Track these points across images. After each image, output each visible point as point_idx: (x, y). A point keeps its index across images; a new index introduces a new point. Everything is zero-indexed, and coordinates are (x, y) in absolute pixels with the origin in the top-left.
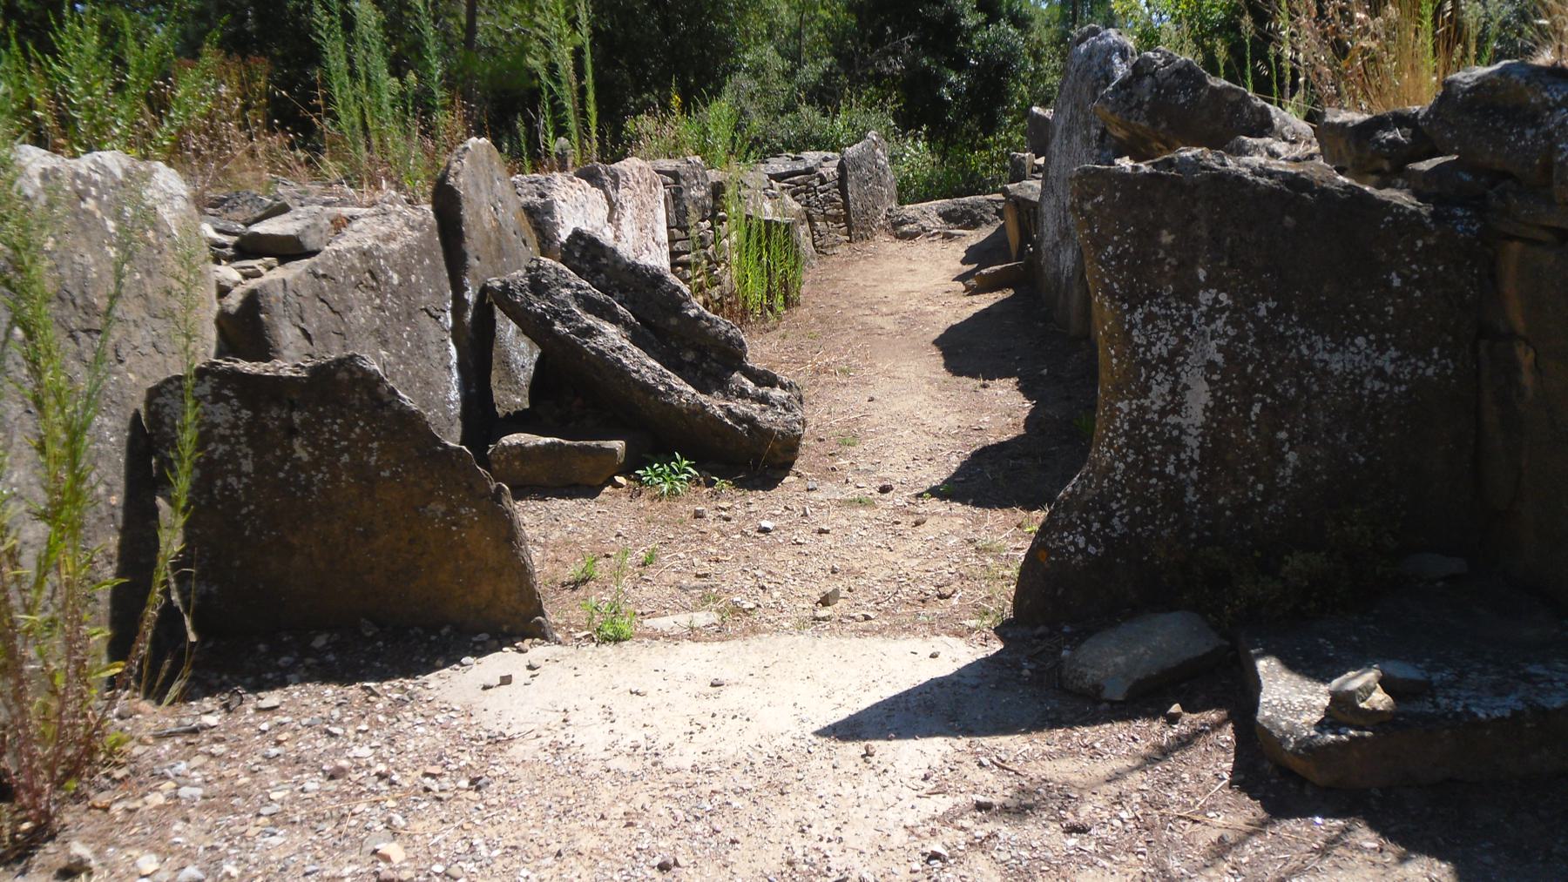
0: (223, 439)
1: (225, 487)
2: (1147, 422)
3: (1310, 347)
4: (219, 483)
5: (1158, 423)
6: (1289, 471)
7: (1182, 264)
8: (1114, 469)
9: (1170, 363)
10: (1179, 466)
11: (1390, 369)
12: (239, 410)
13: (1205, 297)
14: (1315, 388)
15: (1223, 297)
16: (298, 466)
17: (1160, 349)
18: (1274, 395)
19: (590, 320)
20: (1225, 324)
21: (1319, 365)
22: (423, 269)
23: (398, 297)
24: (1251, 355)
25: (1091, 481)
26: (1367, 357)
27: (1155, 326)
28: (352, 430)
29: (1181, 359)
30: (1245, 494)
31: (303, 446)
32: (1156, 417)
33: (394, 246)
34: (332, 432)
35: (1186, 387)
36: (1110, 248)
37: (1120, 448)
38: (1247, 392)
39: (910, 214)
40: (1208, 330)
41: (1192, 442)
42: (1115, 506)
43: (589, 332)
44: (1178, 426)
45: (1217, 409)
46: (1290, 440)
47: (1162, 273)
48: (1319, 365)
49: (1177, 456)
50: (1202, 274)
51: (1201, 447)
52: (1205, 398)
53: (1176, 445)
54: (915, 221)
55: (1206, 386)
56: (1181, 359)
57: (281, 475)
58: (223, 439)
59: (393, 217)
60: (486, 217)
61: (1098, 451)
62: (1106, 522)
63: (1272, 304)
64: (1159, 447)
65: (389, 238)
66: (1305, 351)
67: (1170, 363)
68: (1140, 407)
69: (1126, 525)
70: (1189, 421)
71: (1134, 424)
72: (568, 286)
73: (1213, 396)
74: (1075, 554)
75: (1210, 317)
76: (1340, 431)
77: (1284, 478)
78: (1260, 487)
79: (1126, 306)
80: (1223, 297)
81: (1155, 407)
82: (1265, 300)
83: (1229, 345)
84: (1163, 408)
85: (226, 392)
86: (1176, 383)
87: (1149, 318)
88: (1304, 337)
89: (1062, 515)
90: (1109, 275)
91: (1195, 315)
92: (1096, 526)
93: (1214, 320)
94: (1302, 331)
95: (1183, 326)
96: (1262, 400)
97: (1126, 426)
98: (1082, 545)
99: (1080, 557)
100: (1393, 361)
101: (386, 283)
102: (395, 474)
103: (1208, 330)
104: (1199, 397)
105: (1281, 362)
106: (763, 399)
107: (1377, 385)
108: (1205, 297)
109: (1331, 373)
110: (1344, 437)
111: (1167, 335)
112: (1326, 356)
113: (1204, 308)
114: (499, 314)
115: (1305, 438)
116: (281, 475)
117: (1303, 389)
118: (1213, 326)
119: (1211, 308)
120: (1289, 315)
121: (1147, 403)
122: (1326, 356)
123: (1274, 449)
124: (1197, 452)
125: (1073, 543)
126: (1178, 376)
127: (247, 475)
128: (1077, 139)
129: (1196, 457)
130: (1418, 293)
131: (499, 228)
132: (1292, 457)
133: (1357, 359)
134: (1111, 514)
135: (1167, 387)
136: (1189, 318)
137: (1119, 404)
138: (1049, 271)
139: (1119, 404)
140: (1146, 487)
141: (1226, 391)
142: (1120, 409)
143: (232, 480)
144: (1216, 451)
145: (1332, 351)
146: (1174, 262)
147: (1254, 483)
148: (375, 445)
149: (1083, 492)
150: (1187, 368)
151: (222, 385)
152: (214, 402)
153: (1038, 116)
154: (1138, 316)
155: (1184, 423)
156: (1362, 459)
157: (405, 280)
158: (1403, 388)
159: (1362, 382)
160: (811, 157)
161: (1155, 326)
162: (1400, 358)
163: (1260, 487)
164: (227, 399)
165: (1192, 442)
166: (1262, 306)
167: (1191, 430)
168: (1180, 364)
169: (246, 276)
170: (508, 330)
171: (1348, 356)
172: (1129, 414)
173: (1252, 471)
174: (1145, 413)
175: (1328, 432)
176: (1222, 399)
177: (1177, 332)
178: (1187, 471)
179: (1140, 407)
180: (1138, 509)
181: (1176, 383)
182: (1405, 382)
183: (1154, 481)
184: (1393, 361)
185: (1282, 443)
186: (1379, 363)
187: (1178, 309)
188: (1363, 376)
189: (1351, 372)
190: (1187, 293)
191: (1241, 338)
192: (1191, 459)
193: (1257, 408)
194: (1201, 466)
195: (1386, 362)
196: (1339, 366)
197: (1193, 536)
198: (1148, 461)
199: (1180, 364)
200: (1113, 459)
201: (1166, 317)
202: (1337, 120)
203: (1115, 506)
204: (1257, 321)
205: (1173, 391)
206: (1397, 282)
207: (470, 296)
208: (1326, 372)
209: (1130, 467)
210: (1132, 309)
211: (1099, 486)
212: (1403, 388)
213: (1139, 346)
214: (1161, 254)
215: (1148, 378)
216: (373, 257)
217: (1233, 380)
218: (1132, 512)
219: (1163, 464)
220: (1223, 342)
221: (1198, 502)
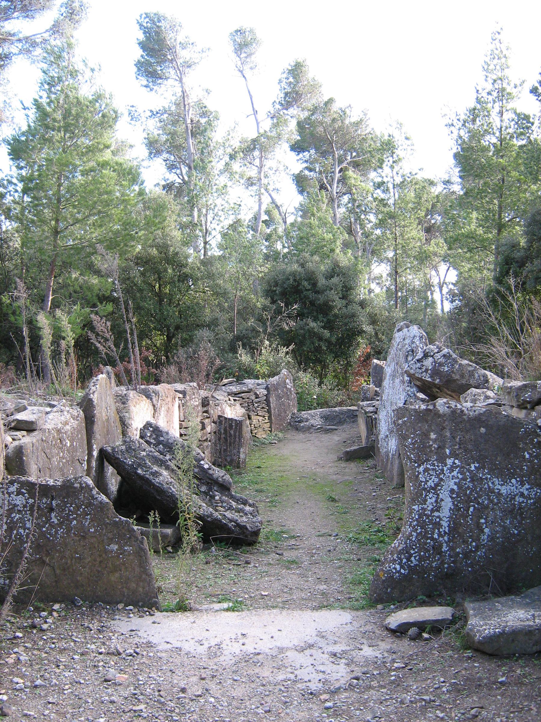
0: (19, 512)
1: (17, 534)
2: (426, 515)
3: (493, 483)
4: (15, 532)
5: (430, 516)
6: (486, 537)
7: (439, 447)
8: (412, 536)
9: (435, 488)
10: (440, 535)
11: (526, 493)
12: (28, 498)
13: (449, 462)
14: (495, 500)
15: (457, 461)
16: (52, 526)
17: (431, 483)
18: (478, 503)
19: (155, 468)
20: (458, 473)
21: (496, 491)
22: (78, 439)
23: (69, 453)
24: (468, 486)
25: (402, 541)
26: (516, 487)
27: (429, 474)
28: (79, 510)
29: (439, 488)
30: (468, 547)
31: (56, 516)
32: (429, 513)
33: (68, 427)
34: (70, 511)
35: (442, 500)
36: (410, 440)
37: (414, 526)
38: (468, 501)
39: (305, 416)
40: (451, 476)
41: (445, 524)
42: (412, 552)
43: (156, 474)
44: (439, 517)
45: (456, 509)
46: (486, 523)
47: (431, 451)
48: (496, 491)
49: (439, 530)
50: (448, 451)
51: (449, 526)
52: (450, 505)
53: (438, 525)
54: (307, 420)
55: (450, 500)
56: (439, 488)
57: (44, 529)
58: (19, 512)
59: (66, 413)
60: (104, 414)
61: (405, 528)
62: (409, 559)
63: (477, 465)
64: (431, 526)
65: (66, 423)
66: (491, 485)
67: (435, 488)
68: (422, 508)
69: (417, 560)
70: (443, 514)
71: (420, 516)
72: (144, 450)
73: (453, 503)
74: (395, 573)
75: (451, 470)
76: (507, 519)
77: (483, 540)
78: (474, 544)
79: (416, 465)
80: (457, 461)
81: (429, 508)
82: (474, 463)
83: (459, 482)
84: (432, 509)
85: (23, 490)
86: (437, 498)
87: (426, 470)
88: (490, 479)
89: (390, 556)
90: (410, 451)
91: (445, 469)
92: (404, 560)
93: (453, 471)
94: (489, 476)
95: (440, 474)
96: (474, 506)
97: (417, 517)
98: (398, 569)
99: (397, 575)
100: (527, 489)
101: (65, 445)
102: (96, 530)
103: (451, 476)
104: (447, 504)
105: (481, 489)
106: (239, 511)
107: (521, 499)
108: (449, 462)
109: (502, 494)
110: (508, 522)
111: (433, 477)
112: (500, 487)
113: (449, 466)
114: (106, 463)
115: (492, 522)
116: (44, 529)
117: (492, 501)
118: (453, 474)
119: (452, 466)
120: (484, 469)
121: (425, 506)
122: (500, 487)
123: (479, 527)
124: (447, 528)
125: (395, 568)
126: (438, 495)
127: (29, 529)
128: (397, 381)
129: (447, 531)
130: (536, 461)
131: (108, 420)
132: (487, 530)
133: (512, 488)
134: (411, 555)
135: (434, 499)
136: (442, 470)
137: (414, 507)
138: (383, 451)
139: (414, 507)
140: (426, 544)
141: (459, 502)
142: (414, 509)
143: (21, 531)
144: (454, 529)
145: (502, 485)
146: (436, 446)
147: (471, 542)
148: (89, 517)
149: (399, 546)
150: (442, 491)
151: (22, 487)
152: (17, 495)
153: (377, 365)
154: (421, 469)
155: (441, 515)
156: (516, 532)
157: (72, 445)
158: (532, 501)
159: (514, 498)
160: (250, 383)
161: (429, 474)
162: (530, 489)
163: (474, 544)
164: (23, 494)
165: (445, 524)
166: (472, 466)
167: (444, 519)
168: (439, 490)
169: (14, 440)
170: (110, 470)
171: (508, 487)
172: (418, 511)
173: (470, 537)
174: (425, 511)
175: (501, 520)
176: (457, 505)
177: (438, 476)
178: (443, 537)
179: (422, 508)
180: (422, 553)
181: (437, 498)
182: (532, 498)
183: (429, 541)
184: (527, 489)
185: (483, 524)
186: (521, 490)
187: (438, 466)
188: (515, 496)
189: (510, 494)
190: (442, 460)
191: (464, 479)
192: (444, 531)
193: (471, 509)
194: (449, 535)
195: (524, 490)
196: (505, 491)
197: (446, 566)
198: (426, 532)
199: (439, 490)
200: (412, 531)
201: (433, 469)
202: (509, 385)
203: (412, 552)
204: (471, 472)
205: (436, 501)
206: (527, 456)
207: (95, 453)
208: (499, 494)
209: (418, 534)
210: (419, 466)
211: (406, 543)
212: (532, 501)
213: (422, 482)
214: (431, 443)
215: (426, 496)
216: (61, 433)
217: (462, 497)
218: (420, 555)
219: (433, 533)
220: (457, 481)
221: (448, 550)
